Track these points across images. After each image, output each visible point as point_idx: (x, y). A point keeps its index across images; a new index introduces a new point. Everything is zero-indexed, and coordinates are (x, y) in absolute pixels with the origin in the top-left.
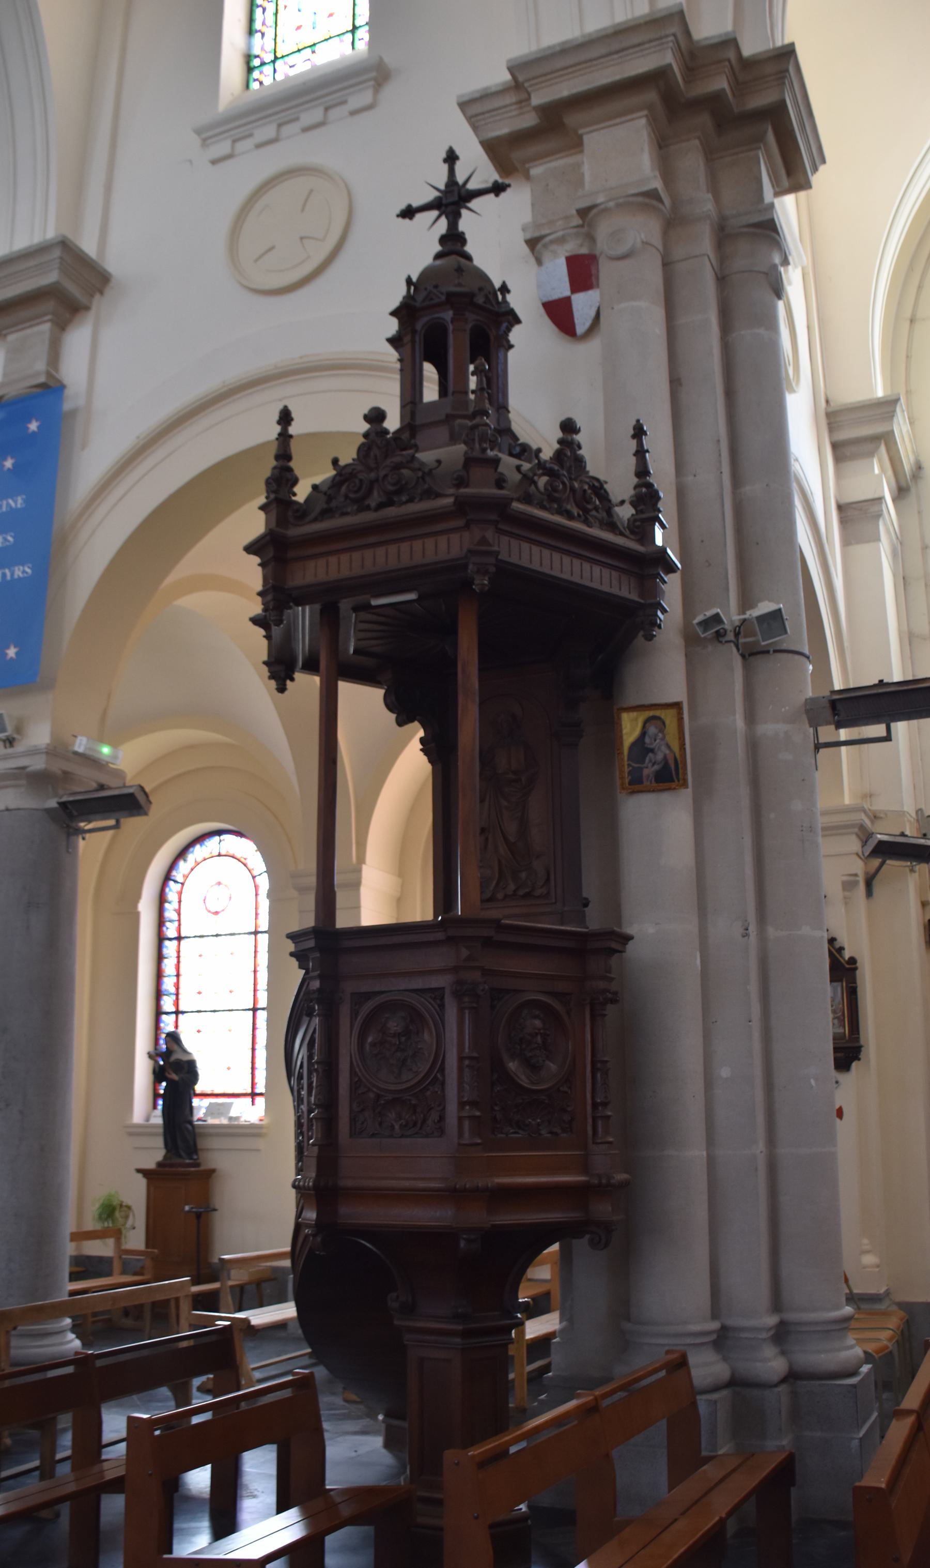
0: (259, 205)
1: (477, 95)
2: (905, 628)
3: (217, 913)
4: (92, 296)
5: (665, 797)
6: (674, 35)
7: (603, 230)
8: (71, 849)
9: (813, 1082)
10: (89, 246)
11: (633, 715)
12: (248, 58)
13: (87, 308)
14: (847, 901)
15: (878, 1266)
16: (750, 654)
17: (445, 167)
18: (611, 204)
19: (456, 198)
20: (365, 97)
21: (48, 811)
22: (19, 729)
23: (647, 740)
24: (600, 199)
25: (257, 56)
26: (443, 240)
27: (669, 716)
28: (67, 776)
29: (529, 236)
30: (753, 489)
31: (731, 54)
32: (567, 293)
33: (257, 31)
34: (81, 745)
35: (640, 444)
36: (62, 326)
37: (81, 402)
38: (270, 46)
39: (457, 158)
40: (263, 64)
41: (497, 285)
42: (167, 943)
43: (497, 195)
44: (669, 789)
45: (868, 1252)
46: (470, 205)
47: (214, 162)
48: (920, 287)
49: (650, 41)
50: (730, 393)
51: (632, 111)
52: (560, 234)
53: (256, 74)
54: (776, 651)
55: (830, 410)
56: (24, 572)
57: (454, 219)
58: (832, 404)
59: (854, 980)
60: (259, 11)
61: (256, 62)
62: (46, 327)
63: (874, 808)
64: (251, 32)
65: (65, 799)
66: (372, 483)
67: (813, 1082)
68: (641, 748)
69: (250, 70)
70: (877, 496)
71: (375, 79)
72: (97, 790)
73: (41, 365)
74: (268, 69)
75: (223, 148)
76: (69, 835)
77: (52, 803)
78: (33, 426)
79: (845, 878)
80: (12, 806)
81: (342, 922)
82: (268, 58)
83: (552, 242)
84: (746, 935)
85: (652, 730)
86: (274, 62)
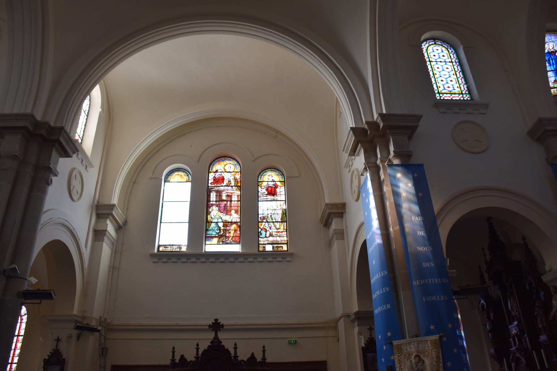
2: (112, 265)
48: (138, 174)
58: (99, 203)
70: (105, 229)
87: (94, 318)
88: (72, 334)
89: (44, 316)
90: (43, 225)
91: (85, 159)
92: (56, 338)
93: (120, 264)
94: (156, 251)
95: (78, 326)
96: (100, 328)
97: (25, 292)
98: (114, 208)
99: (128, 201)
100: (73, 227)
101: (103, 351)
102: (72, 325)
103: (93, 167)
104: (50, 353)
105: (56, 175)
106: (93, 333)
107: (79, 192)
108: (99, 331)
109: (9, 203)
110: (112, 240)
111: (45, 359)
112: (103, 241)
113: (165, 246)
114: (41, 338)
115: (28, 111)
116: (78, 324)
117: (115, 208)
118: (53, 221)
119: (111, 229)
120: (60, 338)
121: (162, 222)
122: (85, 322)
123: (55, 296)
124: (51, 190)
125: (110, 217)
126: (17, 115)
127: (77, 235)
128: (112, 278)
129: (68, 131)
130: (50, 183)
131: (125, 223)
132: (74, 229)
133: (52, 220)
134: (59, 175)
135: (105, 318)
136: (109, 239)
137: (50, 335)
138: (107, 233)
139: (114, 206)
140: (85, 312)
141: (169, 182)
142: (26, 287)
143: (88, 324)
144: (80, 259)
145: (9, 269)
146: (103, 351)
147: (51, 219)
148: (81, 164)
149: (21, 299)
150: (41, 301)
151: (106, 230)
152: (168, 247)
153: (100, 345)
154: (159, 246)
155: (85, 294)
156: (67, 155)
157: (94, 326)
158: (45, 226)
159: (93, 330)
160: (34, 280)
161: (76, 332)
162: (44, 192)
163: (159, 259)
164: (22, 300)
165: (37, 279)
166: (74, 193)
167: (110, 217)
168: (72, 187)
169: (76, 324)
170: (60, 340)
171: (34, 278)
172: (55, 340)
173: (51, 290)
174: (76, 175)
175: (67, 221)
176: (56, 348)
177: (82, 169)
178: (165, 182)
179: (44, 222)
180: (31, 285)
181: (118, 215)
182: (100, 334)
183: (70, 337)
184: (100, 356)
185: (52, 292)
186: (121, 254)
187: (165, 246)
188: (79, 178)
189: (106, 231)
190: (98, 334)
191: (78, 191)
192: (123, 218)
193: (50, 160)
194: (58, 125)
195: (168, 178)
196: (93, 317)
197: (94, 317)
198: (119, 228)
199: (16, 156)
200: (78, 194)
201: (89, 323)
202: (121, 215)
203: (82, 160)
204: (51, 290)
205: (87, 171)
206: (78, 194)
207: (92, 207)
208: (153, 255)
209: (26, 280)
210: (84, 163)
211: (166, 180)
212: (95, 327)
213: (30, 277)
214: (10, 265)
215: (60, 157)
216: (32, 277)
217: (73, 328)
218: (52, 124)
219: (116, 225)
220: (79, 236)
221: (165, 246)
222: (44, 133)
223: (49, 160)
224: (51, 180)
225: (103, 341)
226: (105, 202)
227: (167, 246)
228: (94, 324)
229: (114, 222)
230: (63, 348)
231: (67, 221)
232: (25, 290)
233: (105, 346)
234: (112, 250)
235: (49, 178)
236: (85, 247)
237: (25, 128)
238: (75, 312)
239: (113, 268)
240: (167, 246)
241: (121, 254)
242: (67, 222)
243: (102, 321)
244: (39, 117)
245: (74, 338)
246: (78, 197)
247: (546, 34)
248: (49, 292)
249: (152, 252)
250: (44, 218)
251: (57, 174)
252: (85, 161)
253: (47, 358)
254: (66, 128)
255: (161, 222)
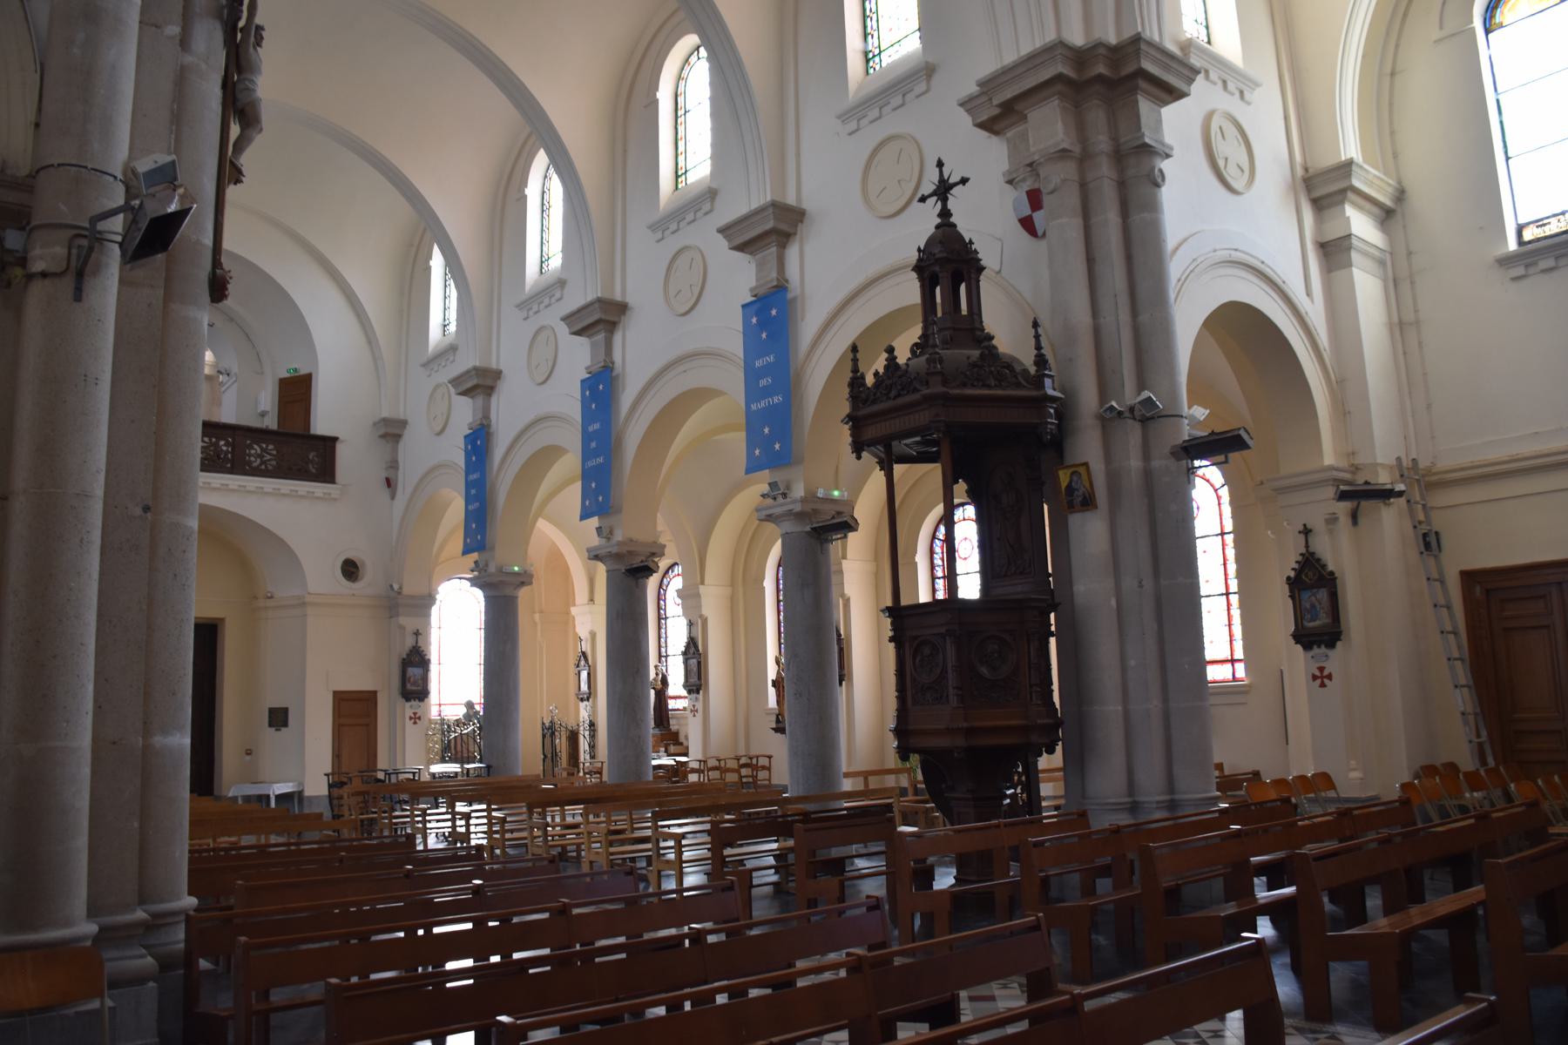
0: (875, 162)
1: (967, 99)
2: (1396, 320)
3: (965, 559)
4: (796, 226)
5: (1088, 514)
6: (1060, 54)
7: (1043, 172)
8: (825, 552)
9: (1186, 666)
10: (791, 200)
11: (1065, 471)
12: (866, 53)
13: (795, 234)
14: (1331, 532)
15: (1361, 779)
16: (1144, 421)
17: (937, 170)
18: (1042, 160)
19: (943, 190)
20: (922, 87)
21: (807, 532)
22: (788, 487)
23: (1073, 484)
24: (1036, 157)
25: (871, 51)
26: (940, 215)
27: (1082, 470)
28: (815, 511)
29: (1006, 179)
30: (1144, 318)
31: (1102, 51)
32: (1029, 212)
33: (869, 34)
34: (821, 493)
35: (1036, 332)
36: (783, 246)
37: (798, 292)
38: (876, 44)
39: (943, 165)
40: (874, 56)
41: (967, 241)
42: (937, 580)
43: (964, 185)
44: (1088, 510)
45: (1354, 770)
46: (951, 192)
47: (850, 134)
48: (1397, 46)
49: (1049, 59)
50: (1129, 258)
51: (1049, 97)
52: (1021, 177)
53: (871, 63)
54: (1159, 417)
55: (1309, 175)
56: (778, 399)
57: (944, 200)
58: (1311, 170)
59: (1335, 586)
60: (869, 20)
61: (871, 55)
62: (774, 249)
63: (1356, 462)
64: (865, 35)
65: (815, 525)
66: (891, 385)
67: (1186, 666)
68: (1070, 489)
69: (868, 61)
70: (1346, 234)
71: (926, 74)
72: (833, 518)
73: (774, 275)
74: (877, 59)
75: (853, 125)
76: (822, 544)
77: (808, 529)
78: (774, 312)
79: (1327, 516)
80: (788, 531)
81: (904, 602)
82: (877, 52)
83: (1019, 181)
84: (1141, 586)
85: (1075, 478)
86: (880, 54)
87: (1381, 464)
88: (1334, 514)
89: (1262, 483)
90: (1181, 282)
91: (1229, 75)
92: (1301, 528)
93: (1416, 311)
94: (1512, 245)
95: (1342, 492)
96: (1400, 487)
97: (1185, 444)
98: (1351, 170)
99: (1392, 133)
100: (1258, 259)
101: (1430, 543)
102: (1330, 492)
103: (1257, 85)
104: (1297, 562)
105: (1168, 156)
106: (1387, 502)
107: (1246, 167)
108: (1400, 494)
109: (1090, 261)
110: (1377, 253)
111: (1289, 578)
112: (1350, 265)
113: (1541, 223)
114: (1269, 532)
115: (1051, 36)
116: (1342, 488)
117: (1354, 168)
118: (1201, 262)
119: (1361, 225)
120: (1309, 527)
121: (1510, 155)
122: (1360, 479)
123: (1252, 438)
124: (1169, 196)
125: (1350, 195)
126: (1031, 57)
127: (1275, 273)
128: (1405, 353)
129: (1156, 38)
130: (1159, 180)
131: (1401, 195)
132: (1263, 262)
133: (1199, 261)
134: (1174, 153)
135: (1414, 457)
136: (1366, 254)
137: (1285, 524)
138: (1354, 241)
139: (1349, 164)
140: (1353, 454)
141: (1501, 26)
142: (1186, 432)
143: (1367, 483)
144: (1304, 331)
145: (1139, 402)
146: (1430, 543)
147: (1194, 260)
148: (1226, 94)
149: (1185, 462)
150: (1226, 457)
151: (1350, 235)
152: (1549, 223)
153: (1415, 527)
154: (1520, 230)
155: (1342, 411)
156: (1174, 94)
157: (1386, 484)
158: (1186, 284)
159: (1386, 495)
160: (1200, 413)
161: (1346, 506)
162: (1153, 206)
163: (1527, 266)
164: (1187, 463)
165: (1206, 408)
166: (1231, 173)
167: (1350, 195)
168: (1221, 163)
169: (1338, 486)
170: (1311, 531)
171: (1199, 408)
172: (1300, 532)
173: (1239, 429)
174: (1220, 128)
175: (1236, 250)
176: (1307, 550)
177: (1230, 104)
178: (1487, 32)
179: (1182, 275)
180: (1195, 423)
181: (1371, 184)
182: (1408, 501)
183: (1332, 520)
184: (1422, 553)
185: (1242, 433)
186: (1412, 283)
187: (1541, 223)
188: (1231, 131)
189: (1351, 238)
190: (1402, 501)
191: (1240, 165)
192: (1389, 185)
193: (1140, 128)
194: (1128, 34)
195: (1492, 17)
196: (1377, 464)
197: (1379, 461)
198: (1386, 216)
199: (1064, 150)
200: (1242, 171)
201: (1369, 480)
202: (1382, 180)
203: (1225, 82)
204: (1239, 429)
205: (1249, 103)
206: (1242, 171)
207: (1293, 188)
208: (1507, 261)
209: (1182, 416)
210: (1231, 86)
211: (1490, 25)
212: (1389, 487)
213: (1190, 408)
214: (1139, 394)
215: (1162, 107)
216: (1195, 407)
217: (1334, 499)
218: (1112, 40)
219: (1375, 210)
220: (1279, 273)
221: (1539, 223)
222: (1101, 69)
223: (1139, 127)
224: (1161, 171)
225: (1421, 517)
226: (1326, 161)
227: (1545, 222)
228: (1383, 479)
229: (1368, 206)
230: (1323, 548)
231: (1236, 250)
232: (1184, 441)
233: (1428, 528)
234: (1385, 281)
235: (1153, 169)
236: (1308, 295)
237: (1059, 78)
238: (1329, 459)
239: (1402, 327)
240: (1545, 222)
241: (1412, 283)
242: (1238, 254)
243: (1409, 470)
244: (1077, 38)
245: (1344, 520)
246: (1246, 182)
247: (1258, 918)
248: (1236, 433)
249: (1500, 252)
250: (1175, 269)
251: (1167, 151)
252: (1235, 81)
253: (1292, 574)
254: (1147, 35)
255: (1508, 158)
